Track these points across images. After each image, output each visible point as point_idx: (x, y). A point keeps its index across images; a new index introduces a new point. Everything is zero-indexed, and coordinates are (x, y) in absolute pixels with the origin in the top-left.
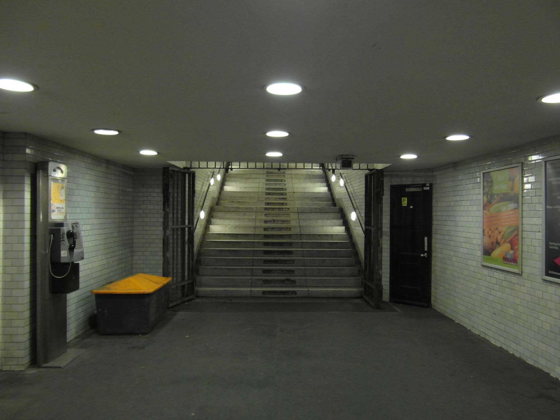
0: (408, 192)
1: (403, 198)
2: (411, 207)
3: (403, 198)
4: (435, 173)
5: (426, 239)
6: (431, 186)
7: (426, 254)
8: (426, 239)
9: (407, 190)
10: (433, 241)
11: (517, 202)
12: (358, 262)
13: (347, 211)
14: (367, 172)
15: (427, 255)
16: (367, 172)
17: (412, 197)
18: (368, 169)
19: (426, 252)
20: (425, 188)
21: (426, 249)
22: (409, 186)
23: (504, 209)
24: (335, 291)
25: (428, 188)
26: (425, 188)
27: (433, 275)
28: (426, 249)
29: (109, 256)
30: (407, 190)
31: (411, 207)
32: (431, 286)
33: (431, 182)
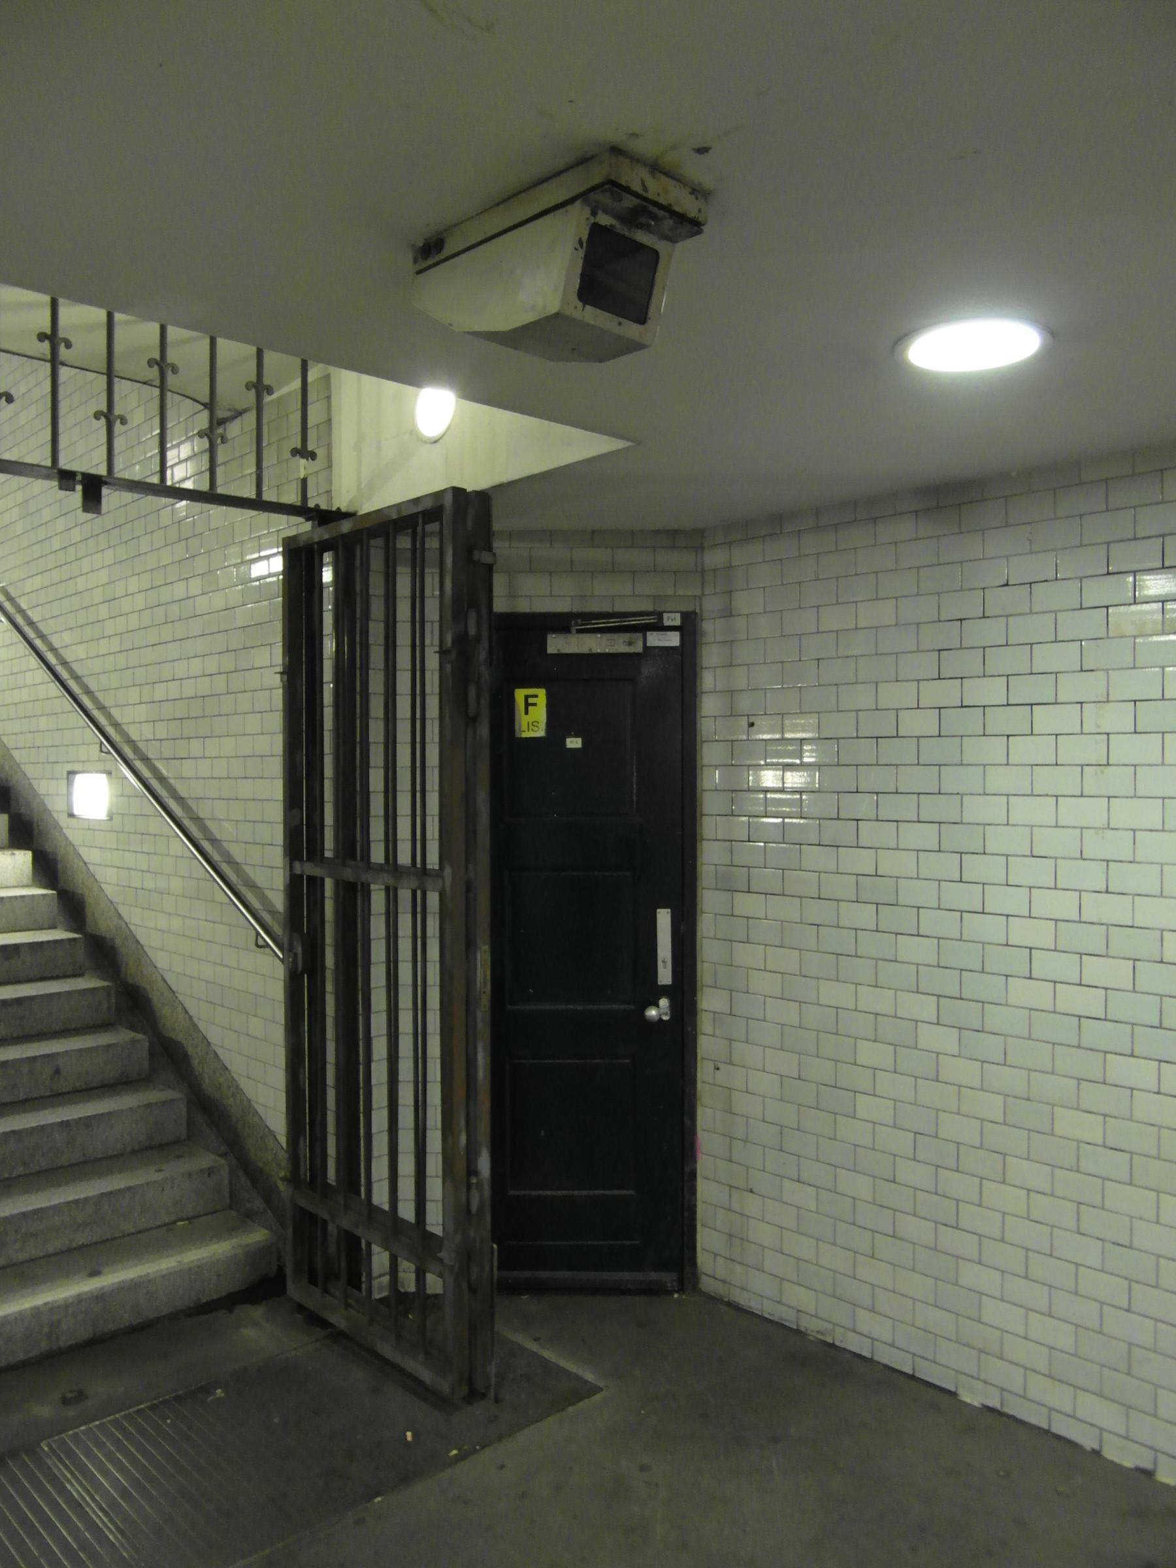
0: (560, 657)
1: (520, 694)
2: (574, 743)
3: (520, 694)
4: (714, 558)
5: (664, 918)
6: (690, 626)
7: (664, 1002)
8: (664, 918)
9: (557, 644)
10: (706, 925)
11: (189, 1137)
12: (211, 1114)
13: (43, 787)
14: (300, 527)
15: (673, 1007)
16: (300, 527)
17: (570, 681)
18: (301, 510)
19: (665, 991)
20: (655, 639)
21: (665, 976)
22: (562, 623)
23: (21, 1169)
24: (100, 1297)
25: (673, 640)
26: (655, 639)
27: (707, 1117)
28: (665, 976)
29: (952, 780)
30: (557, 644)
31: (574, 743)
32: (693, 1175)
33: (688, 608)
